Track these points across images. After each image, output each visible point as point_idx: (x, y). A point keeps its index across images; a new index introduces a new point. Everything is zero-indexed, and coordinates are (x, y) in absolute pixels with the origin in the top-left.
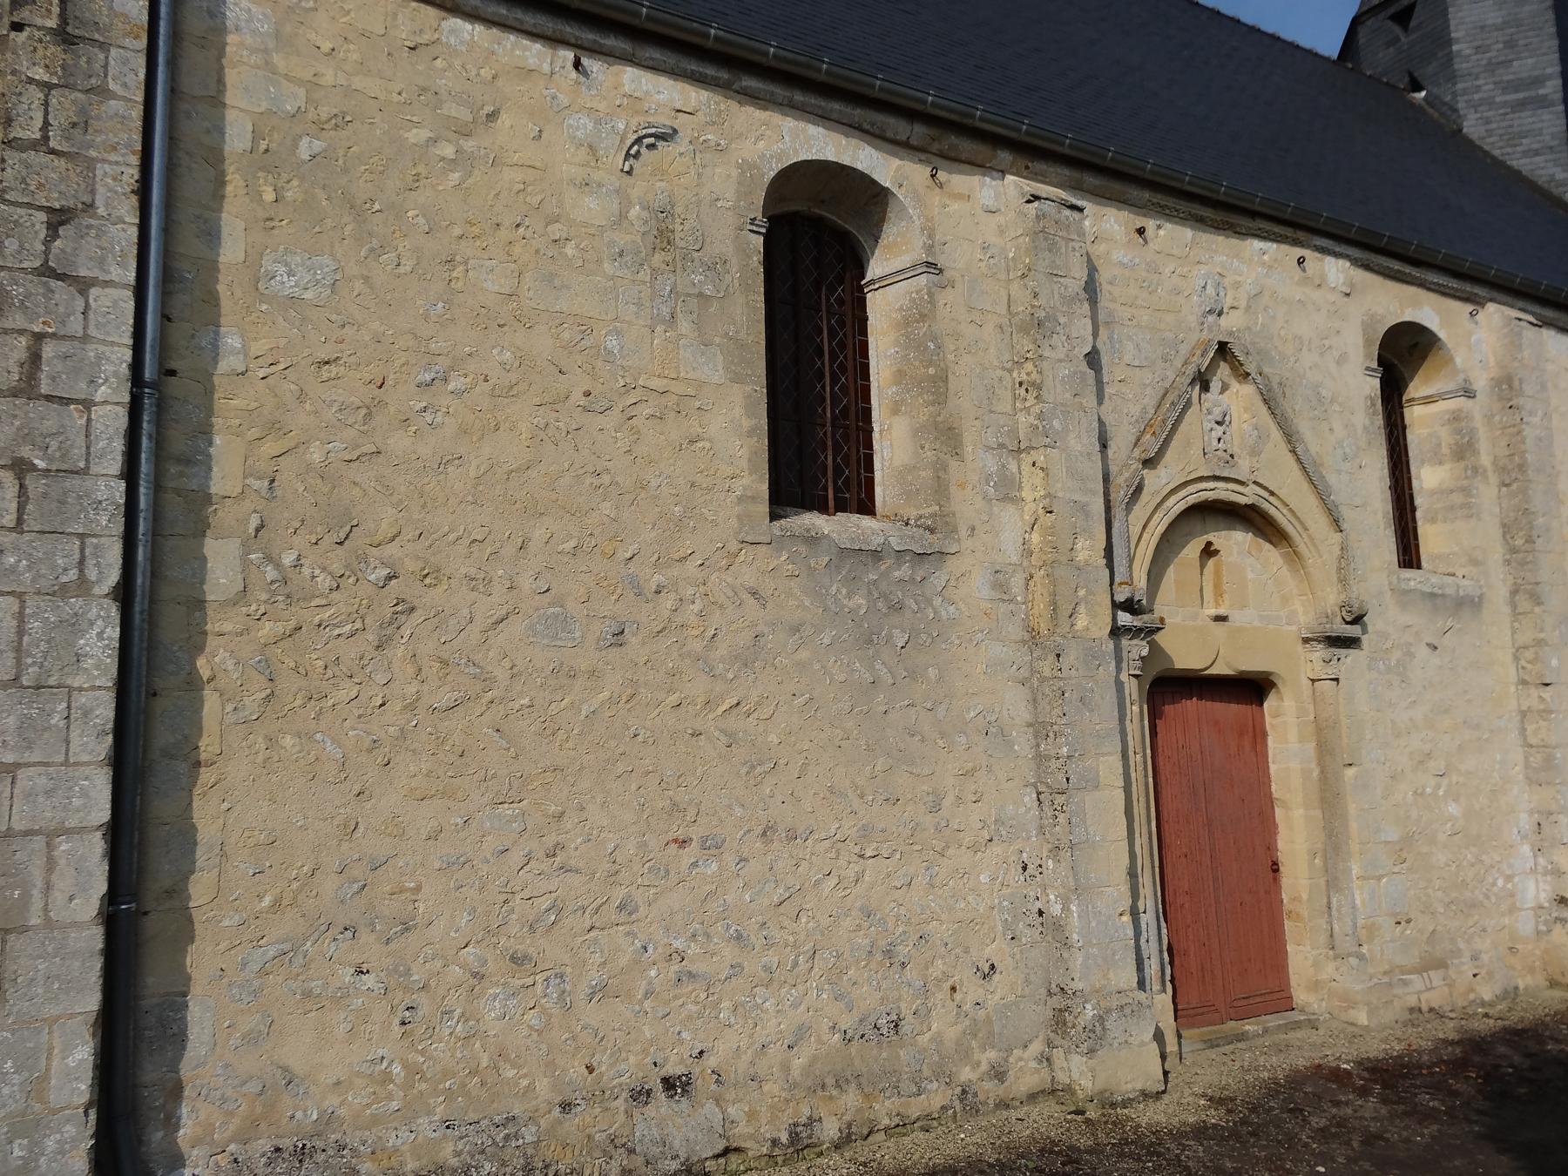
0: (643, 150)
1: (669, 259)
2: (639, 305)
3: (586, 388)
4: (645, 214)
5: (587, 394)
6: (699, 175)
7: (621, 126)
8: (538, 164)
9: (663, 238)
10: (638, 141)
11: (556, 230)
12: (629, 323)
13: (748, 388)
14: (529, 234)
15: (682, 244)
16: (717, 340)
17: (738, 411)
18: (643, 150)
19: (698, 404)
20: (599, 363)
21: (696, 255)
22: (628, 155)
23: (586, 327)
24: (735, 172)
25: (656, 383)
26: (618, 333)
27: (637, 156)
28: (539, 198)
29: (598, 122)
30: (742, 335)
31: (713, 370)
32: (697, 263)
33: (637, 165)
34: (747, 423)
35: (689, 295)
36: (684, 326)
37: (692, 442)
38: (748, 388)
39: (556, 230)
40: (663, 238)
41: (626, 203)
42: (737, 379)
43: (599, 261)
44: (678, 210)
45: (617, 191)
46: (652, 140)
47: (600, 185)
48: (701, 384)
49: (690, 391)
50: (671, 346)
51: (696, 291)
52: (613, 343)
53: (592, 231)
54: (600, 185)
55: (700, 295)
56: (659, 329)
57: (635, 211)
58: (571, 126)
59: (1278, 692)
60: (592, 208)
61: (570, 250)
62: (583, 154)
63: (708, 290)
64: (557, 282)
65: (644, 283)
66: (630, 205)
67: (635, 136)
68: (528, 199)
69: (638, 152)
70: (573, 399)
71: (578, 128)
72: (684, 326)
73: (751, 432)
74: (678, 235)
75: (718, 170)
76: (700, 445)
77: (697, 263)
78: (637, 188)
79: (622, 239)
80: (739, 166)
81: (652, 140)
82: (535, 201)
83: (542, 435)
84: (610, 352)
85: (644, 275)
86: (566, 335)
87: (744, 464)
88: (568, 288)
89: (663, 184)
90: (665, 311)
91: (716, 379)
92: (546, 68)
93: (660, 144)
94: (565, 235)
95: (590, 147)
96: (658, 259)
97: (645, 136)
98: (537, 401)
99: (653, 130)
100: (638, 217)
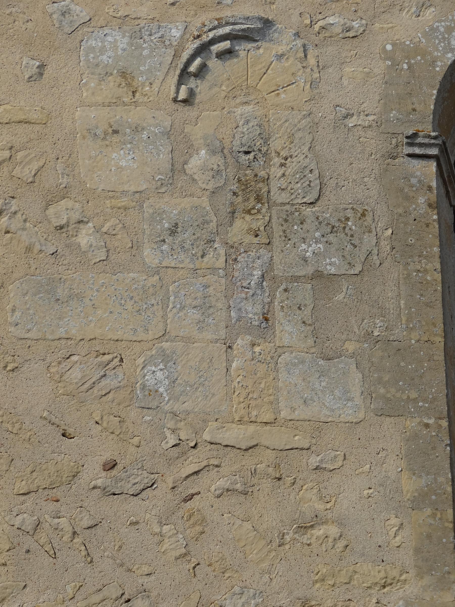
0: (213, 63)
1: (260, 224)
2: (205, 307)
3: (107, 456)
4: (216, 161)
5: (110, 466)
6: (313, 84)
7: (176, 33)
8: (33, 116)
9: (250, 192)
10: (203, 49)
11: (62, 211)
12: (188, 340)
13: (412, 424)
14: (15, 224)
15: (284, 197)
16: (351, 347)
17: (393, 465)
18: (213, 63)
19: (314, 461)
20: (133, 414)
21: (308, 211)
22: (184, 74)
23: (111, 357)
24: (380, 67)
25: (234, 434)
26: (167, 358)
27: (202, 71)
28: (35, 166)
29: (136, 35)
30: (398, 332)
31: (340, 398)
32: (310, 224)
33: (201, 87)
34: (410, 485)
35: (295, 279)
36: (287, 330)
37: (304, 528)
38: (412, 424)
39: (62, 211)
40: (250, 192)
41: (182, 147)
42: (390, 409)
43: (135, 247)
44: (276, 144)
45: (167, 134)
46: (226, 44)
47: (137, 129)
48: (319, 427)
49: (300, 440)
50: (262, 368)
51: (310, 270)
52: (156, 376)
53: (124, 201)
54: (137, 129)
55: (318, 275)
56: (241, 342)
57: (199, 160)
58: (92, 49)
59: (203, 81)
60: (125, 167)
61: (85, 238)
62: (111, 88)
63: (332, 265)
64: (61, 292)
65: (213, 270)
66: (191, 149)
67: (197, 43)
68: (17, 172)
69: (203, 67)
70: (85, 477)
71: (103, 50)
72: (287, 330)
73: (419, 500)
74: (274, 185)
75: (348, 69)
76: (319, 532)
77: (310, 224)
78: (203, 124)
79: (174, 206)
80: (387, 56)
81: (226, 44)
82: (26, 173)
83: (28, 542)
84: (153, 392)
85: (217, 257)
86: (75, 375)
87: (407, 558)
88: (80, 297)
89: (249, 108)
90: (252, 311)
91: (348, 414)
92: (165, 429)
93: (242, 47)
94: (76, 216)
95: (123, 74)
96: (239, 228)
97: (213, 42)
98: (23, 487)
99: (227, 29)
100: (204, 169)
